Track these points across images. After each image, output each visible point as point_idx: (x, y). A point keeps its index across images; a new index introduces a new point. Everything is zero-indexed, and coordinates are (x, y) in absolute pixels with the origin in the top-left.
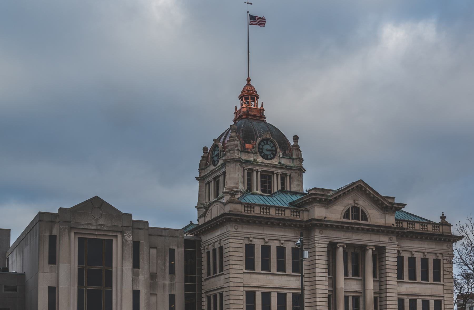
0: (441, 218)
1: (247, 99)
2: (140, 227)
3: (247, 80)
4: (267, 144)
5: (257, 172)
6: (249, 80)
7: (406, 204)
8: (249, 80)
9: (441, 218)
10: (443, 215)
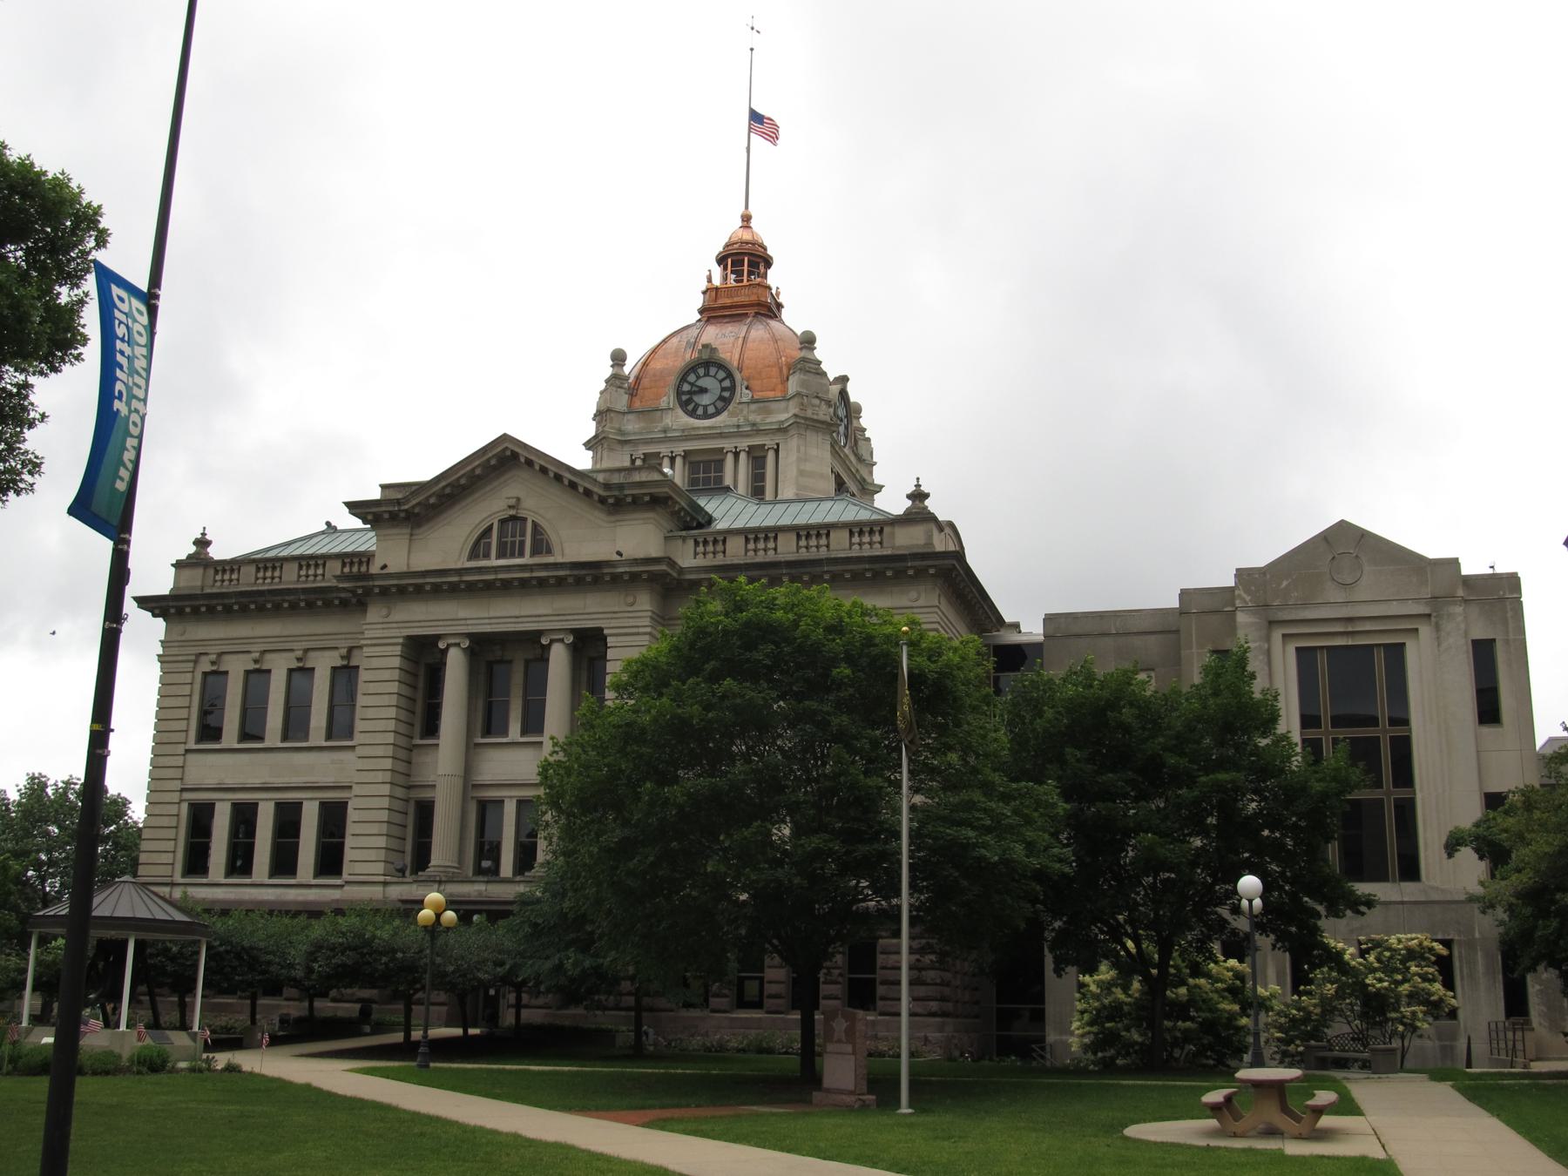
0: (197, 542)
1: (737, 263)
2: (1153, 637)
4: (707, 374)
5: (736, 455)
6: (746, 219)
7: (348, 504)
8: (746, 219)
9: (197, 542)
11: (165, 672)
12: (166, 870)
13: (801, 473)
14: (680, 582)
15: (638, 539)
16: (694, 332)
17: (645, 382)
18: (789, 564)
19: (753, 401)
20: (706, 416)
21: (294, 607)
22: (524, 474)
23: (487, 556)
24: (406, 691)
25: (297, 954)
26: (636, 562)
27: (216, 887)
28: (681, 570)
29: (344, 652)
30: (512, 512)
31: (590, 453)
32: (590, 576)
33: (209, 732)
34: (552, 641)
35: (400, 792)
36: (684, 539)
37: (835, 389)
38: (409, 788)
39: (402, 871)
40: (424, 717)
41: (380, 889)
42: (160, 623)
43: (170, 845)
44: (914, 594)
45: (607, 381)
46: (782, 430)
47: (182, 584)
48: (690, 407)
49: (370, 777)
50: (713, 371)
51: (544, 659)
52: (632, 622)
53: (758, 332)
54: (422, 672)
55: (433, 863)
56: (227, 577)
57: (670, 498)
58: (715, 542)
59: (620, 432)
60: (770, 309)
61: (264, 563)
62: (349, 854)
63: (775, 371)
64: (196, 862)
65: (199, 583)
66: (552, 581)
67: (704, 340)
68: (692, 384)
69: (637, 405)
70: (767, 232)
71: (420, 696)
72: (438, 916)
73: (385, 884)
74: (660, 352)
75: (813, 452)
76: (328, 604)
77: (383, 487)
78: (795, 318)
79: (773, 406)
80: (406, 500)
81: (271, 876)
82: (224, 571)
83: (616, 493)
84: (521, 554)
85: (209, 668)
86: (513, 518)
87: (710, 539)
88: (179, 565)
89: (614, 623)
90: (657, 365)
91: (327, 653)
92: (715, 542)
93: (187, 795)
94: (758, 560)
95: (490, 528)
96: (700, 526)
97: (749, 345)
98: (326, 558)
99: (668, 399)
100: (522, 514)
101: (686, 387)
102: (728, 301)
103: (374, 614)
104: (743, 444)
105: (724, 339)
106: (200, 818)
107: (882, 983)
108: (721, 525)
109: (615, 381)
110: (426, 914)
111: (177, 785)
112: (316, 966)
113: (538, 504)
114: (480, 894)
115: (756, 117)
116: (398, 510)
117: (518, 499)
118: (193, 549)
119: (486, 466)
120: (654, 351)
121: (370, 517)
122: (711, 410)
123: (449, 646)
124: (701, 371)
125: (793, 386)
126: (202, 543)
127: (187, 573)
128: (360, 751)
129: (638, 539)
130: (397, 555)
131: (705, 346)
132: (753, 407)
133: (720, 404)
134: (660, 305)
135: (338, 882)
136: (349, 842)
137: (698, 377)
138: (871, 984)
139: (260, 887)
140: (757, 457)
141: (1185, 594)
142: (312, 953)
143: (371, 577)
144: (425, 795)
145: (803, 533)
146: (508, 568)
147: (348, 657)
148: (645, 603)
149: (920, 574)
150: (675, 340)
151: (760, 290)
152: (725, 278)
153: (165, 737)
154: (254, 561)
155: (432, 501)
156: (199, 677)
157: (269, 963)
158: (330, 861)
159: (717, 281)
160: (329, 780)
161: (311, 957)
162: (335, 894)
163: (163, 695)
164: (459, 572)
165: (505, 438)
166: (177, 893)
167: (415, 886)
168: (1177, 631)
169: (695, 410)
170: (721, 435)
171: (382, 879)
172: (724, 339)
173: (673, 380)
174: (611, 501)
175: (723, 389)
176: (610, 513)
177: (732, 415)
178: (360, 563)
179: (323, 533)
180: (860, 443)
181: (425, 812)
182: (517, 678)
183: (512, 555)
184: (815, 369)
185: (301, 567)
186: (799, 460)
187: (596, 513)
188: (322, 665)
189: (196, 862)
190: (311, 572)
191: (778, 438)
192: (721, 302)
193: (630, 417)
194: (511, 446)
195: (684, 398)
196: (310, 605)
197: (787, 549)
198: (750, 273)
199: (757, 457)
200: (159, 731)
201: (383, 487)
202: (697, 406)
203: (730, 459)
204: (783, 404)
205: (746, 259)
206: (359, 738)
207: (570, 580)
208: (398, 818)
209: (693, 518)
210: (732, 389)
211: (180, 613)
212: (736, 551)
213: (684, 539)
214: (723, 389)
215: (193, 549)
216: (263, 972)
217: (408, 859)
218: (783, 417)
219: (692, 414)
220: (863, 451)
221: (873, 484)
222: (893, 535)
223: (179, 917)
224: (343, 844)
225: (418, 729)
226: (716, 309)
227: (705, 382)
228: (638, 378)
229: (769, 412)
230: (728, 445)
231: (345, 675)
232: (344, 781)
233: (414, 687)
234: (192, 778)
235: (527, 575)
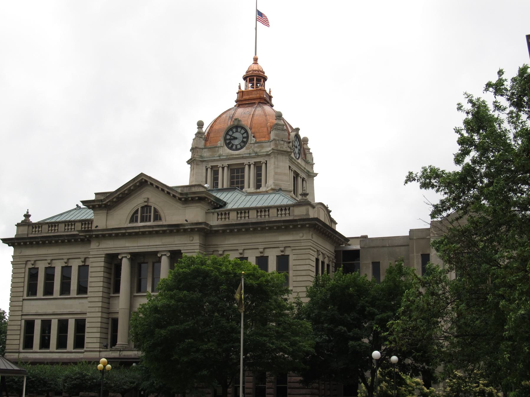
0: (25, 216)
2: (403, 248)
3: (254, 59)
4: (237, 131)
5: (249, 166)
6: (256, 60)
8: (256, 60)
9: (25, 216)
10: (28, 212)
11: (14, 268)
12: (17, 347)
13: (276, 173)
14: (211, 231)
15: (194, 214)
16: (232, 112)
17: (212, 135)
18: (253, 224)
19: (256, 143)
20: (237, 149)
21: (63, 242)
22: (149, 188)
23: (137, 221)
24: (106, 275)
25: (60, 380)
26: (193, 224)
27: (36, 353)
29: (83, 259)
30: (146, 204)
31: (189, 166)
32: (176, 230)
33: (32, 290)
34: (162, 255)
35: (105, 315)
36: (213, 213)
37: (293, 134)
38: (109, 313)
39: (106, 347)
40: (113, 285)
41: (98, 353)
42: (12, 248)
43: (18, 337)
44: (301, 235)
45: (196, 135)
46: (268, 155)
47: (20, 233)
48: (230, 146)
49: (93, 310)
50: (239, 130)
51: (159, 261)
52: (192, 248)
53: (259, 111)
54: (113, 267)
55: (118, 343)
56: (37, 230)
57: (206, 198)
58: (225, 214)
59: (201, 157)
60: (267, 100)
61: (51, 224)
62: (86, 340)
63: (266, 129)
64: (28, 343)
65: (26, 233)
67: (237, 116)
68: (231, 136)
69: (208, 145)
70: (264, 65)
71: (112, 277)
72: (105, 366)
73: (100, 351)
75: (281, 164)
76: (76, 241)
77: (96, 194)
78: (278, 104)
79: (264, 144)
80: (104, 200)
81: (57, 348)
82: (36, 227)
83: (185, 196)
85: (31, 266)
86: (146, 206)
87: (223, 213)
88: (18, 225)
90: (216, 127)
91: (77, 260)
93: (24, 317)
95: (137, 212)
96: (221, 207)
97: (255, 118)
98: (75, 222)
100: (150, 204)
101: (228, 137)
103: (94, 245)
104: (252, 161)
106: (29, 325)
107: (290, 388)
108: (229, 207)
109: (199, 134)
110: (100, 366)
111: (20, 313)
112: (66, 384)
113: (156, 201)
114: (135, 355)
115: (260, 14)
116: (104, 203)
118: (24, 218)
119: (135, 185)
120: (215, 121)
121: (91, 207)
122: (239, 147)
123: (122, 257)
124: (234, 130)
126: (27, 216)
127: (22, 228)
128: (89, 299)
129: (194, 214)
130: (101, 221)
131: (236, 119)
132: (256, 145)
133: (242, 144)
134: (219, 100)
135: (83, 351)
136: (86, 335)
137: (233, 133)
138: (286, 388)
139: (53, 353)
140: (258, 167)
141: (411, 231)
142: (65, 380)
143: (92, 231)
144: (115, 316)
145: (259, 210)
146: (144, 227)
147: (84, 261)
148: (197, 240)
149: (303, 227)
150: (224, 116)
151: (261, 92)
152: (246, 86)
153: (15, 294)
154: (47, 223)
155: (115, 200)
156: (27, 270)
157: (51, 384)
158: (79, 343)
159: (243, 89)
160: (78, 311)
161: (65, 381)
162: (81, 356)
163: (13, 277)
165: (142, 174)
166: (22, 356)
167: (110, 352)
168: (408, 245)
169: (232, 146)
170: (243, 158)
171: (98, 349)
173: (223, 134)
174: (183, 199)
175: (244, 138)
176: (183, 204)
177: (247, 149)
178: (89, 224)
179: (75, 209)
180: (308, 155)
181: (115, 322)
182: (150, 269)
183: (146, 221)
185: (65, 226)
186: (275, 168)
188: (75, 265)
189: (28, 343)
190: (70, 227)
191: (266, 159)
193: (205, 150)
194: (145, 178)
195: (228, 141)
196: (69, 241)
197: (253, 217)
199: (258, 167)
200: (12, 292)
201: (96, 194)
202: (233, 145)
203: (247, 168)
204: (269, 143)
205: (255, 77)
206: (89, 294)
207: (168, 231)
208: (104, 326)
209: (217, 204)
210: (247, 137)
211: (19, 244)
212: (233, 218)
213: (213, 213)
214: (244, 138)
215: (24, 218)
216: (49, 387)
217: (109, 341)
219: (231, 148)
220: (308, 158)
221: (313, 173)
222: (293, 210)
223: (16, 368)
224: (84, 336)
225: (112, 290)
226: (243, 100)
227: (236, 135)
228: (209, 133)
229: (263, 147)
230: (246, 161)
231: (83, 270)
232: (84, 311)
233: (110, 273)
234: (26, 310)
235: (151, 230)
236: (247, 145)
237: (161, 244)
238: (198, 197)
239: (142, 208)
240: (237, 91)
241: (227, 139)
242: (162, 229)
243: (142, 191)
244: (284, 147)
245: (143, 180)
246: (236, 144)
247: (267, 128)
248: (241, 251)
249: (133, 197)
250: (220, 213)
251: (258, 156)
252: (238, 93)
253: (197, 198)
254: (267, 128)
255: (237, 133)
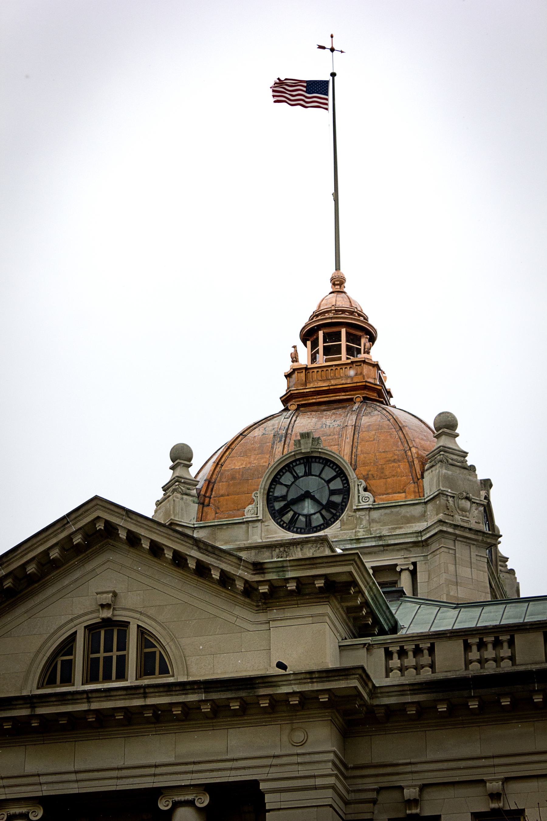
4: (308, 473)
6: (338, 283)
8: (338, 283)
14: (371, 710)
15: (304, 643)
17: (221, 488)
26: (311, 676)
28: (374, 691)
30: (106, 614)
32: (239, 700)
34: (177, 805)
45: (165, 488)
46: (421, 544)
50: (316, 468)
53: (371, 418)
60: (376, 394)
63: (403, 467)
66: (177, 711)
70: (366, 298)
74: (237, 448)
84: (121, 676)
86: (107, 623)
89: (274, 773)
90: (235, 464)
92: (418, 651)
94: (490, 668)
95: (68, 646)
99: (256, 508)
100: (121, 616)
102: (323, 385)
105: (327, 428)
117: (115, 595)
120: (229, 447)
124: (317, 460)
125: (431, 484)
129: (304, 643)
132: (375, 514)
134: (231, 389)
137: (296, 478)
150: (257, 433)
151: (366, 369)
152: (314, 358)
164: (31, 701)
165: (96, 502)
172: (327, 428)
173: (263, 482)
175: (333, 492)
184: (458, 461)
187: (238, 611)
191: (415, 556)
192: (312, 386)
195: (278, 506)
198: (350, 351)
204: (419, 509)
205: (339, 332)
210: (346, 492)
218: (421, 526)
228: (209, 482)
235: (138, 702)
236: (344, 516)
237: (172, 759)
238: (325, 576)
239: (92, 629)
240: (288, 370)
241: (277, 499)
242: (181, 699)
243: (89, 567)
244: (473, 521)
245: (100, 526)
246: (305, 512)
247: (411, 465)
248: (494, 786)
249: (50, 591)
250: (394, 649)
251: (386, 548)
252: (288, 376)
253: (320, 583)
254: (411, 465)
255: (300, 482)
